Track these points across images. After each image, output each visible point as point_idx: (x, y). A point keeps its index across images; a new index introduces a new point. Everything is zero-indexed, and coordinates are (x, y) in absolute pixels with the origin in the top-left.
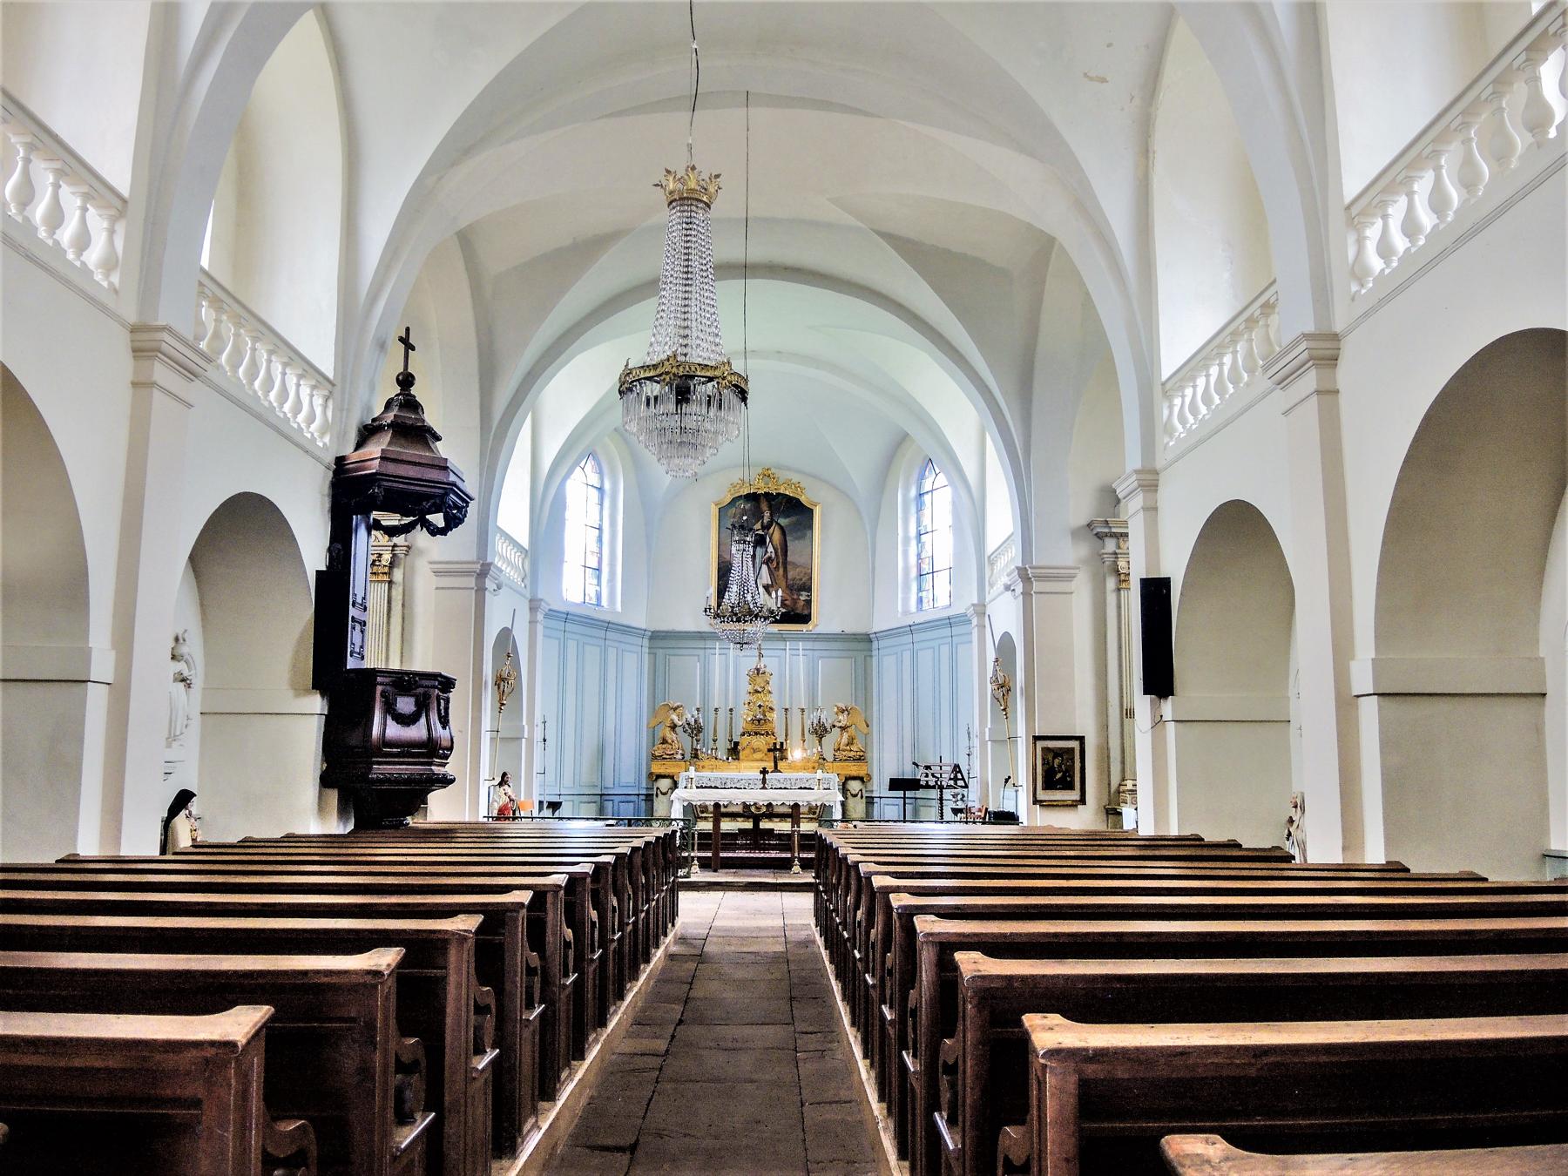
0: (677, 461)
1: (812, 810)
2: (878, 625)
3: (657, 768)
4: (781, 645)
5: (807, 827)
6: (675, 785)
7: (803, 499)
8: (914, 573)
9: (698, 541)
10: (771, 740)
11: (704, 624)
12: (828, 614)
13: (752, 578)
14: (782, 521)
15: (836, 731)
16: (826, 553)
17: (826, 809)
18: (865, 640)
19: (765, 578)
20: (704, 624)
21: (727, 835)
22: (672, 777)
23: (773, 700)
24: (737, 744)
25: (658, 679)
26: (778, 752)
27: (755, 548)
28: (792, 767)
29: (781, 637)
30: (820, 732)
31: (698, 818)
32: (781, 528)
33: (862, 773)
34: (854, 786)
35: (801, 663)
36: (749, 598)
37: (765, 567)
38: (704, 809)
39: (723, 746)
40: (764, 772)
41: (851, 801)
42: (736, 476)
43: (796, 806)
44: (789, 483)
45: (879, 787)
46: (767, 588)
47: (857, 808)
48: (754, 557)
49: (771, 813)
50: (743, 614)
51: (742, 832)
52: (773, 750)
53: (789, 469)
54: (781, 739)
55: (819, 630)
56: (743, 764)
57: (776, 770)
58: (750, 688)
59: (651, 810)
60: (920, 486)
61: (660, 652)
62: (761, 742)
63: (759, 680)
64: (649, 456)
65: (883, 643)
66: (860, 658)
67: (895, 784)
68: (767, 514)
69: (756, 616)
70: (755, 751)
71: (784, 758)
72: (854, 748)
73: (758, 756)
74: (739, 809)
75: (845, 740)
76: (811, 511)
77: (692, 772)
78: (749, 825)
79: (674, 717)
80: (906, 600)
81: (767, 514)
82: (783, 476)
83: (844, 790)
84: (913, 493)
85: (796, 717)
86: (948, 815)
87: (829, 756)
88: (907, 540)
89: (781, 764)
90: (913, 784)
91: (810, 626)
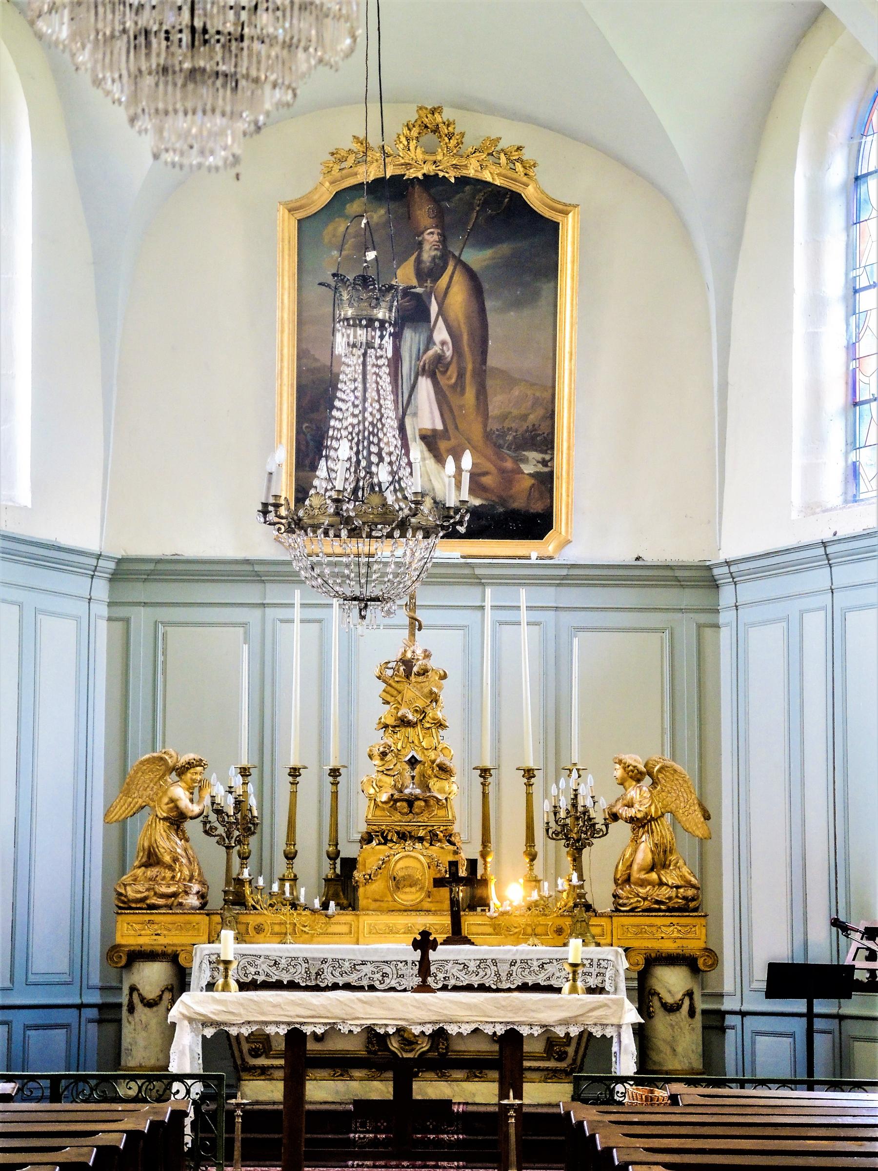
0: (182, 123)
1: (554, 1045)
2: (737, 540)
3: (132, 933)
4: (467, 595)
5: (539, 1094)
6: (180, 982)
7: (531, 195)
8: (836, 397)
9: (239, 311)
10: (442, 854)
11: (262, 543)
12: (591, 525)
13: (391, 422)
14: (477, 257)
15: (621, 831)
16: (595, 342)
17: (593, 1047)
18: (704, 579)
19: (427, 414)
20: (262, 543)
21: (333, 1119)
22: (172, 958)
23: (452, 746)
24: (350, 864)
25: (133, 687)
26: (463, 887)
27: (397, 337)
28: (501, 929)
29: (468, 576)
30: (577, 831)
31: (243, 1071)
32: (472, 275)
33: (694, 946)
34: (672, 982)
35: (524, 641)
36: (383, 474)
37: (425, 385)
38: (261, 1042)
39: (312, 867)
40: (424, 943)
41: (662, 1024)
42: (346, 129)
43: (511, 1039)
44: (490, 150)
45: (740, 983)
46: (430, 440)
47: (681, 1042)
48: (396, 361)
49: (441, 1052)
50: (369, 515)
51: (365, 1108)
52: (448, 879)
53: (492, 109)
54: (470, 850)
55: (575, 554)
56: (367, 921)
57: (457, 936)
58: (385, 713)
59: (114, 1052)
60: (856, 155)
61: (141, 618)
62: (414, 860)
63: (411, 691)
64: (109, 105)
65: (748, 591)
66: (686, 627)
67: (785, 979)
68: (431, 238)
69: (403, 526)
70: (398, 883)
71: (478, 903)
72: (670, 878)
73: (409, 896)
74: (355, 1046)
75: (644, 854)
76: (554, 227)
77: (228, 945)
78: (381, 1090)
79: (180, 793)
80: (812, 472)
81: (431, 238)
82: (475, 128)
83: (643, 994)
84: (837, 173)
85: (510, 791)
86: (234, 985)
87: (601, 895)
88: (817, 304)
89: (471, 922)
90: (834, 980)
91: (548, 545)
